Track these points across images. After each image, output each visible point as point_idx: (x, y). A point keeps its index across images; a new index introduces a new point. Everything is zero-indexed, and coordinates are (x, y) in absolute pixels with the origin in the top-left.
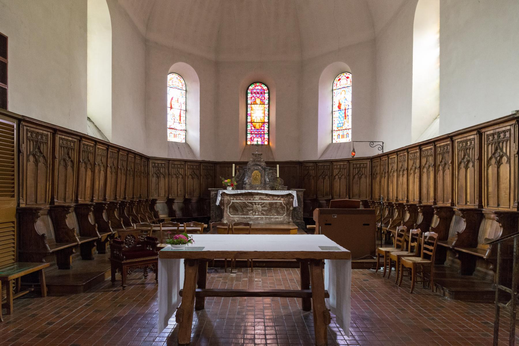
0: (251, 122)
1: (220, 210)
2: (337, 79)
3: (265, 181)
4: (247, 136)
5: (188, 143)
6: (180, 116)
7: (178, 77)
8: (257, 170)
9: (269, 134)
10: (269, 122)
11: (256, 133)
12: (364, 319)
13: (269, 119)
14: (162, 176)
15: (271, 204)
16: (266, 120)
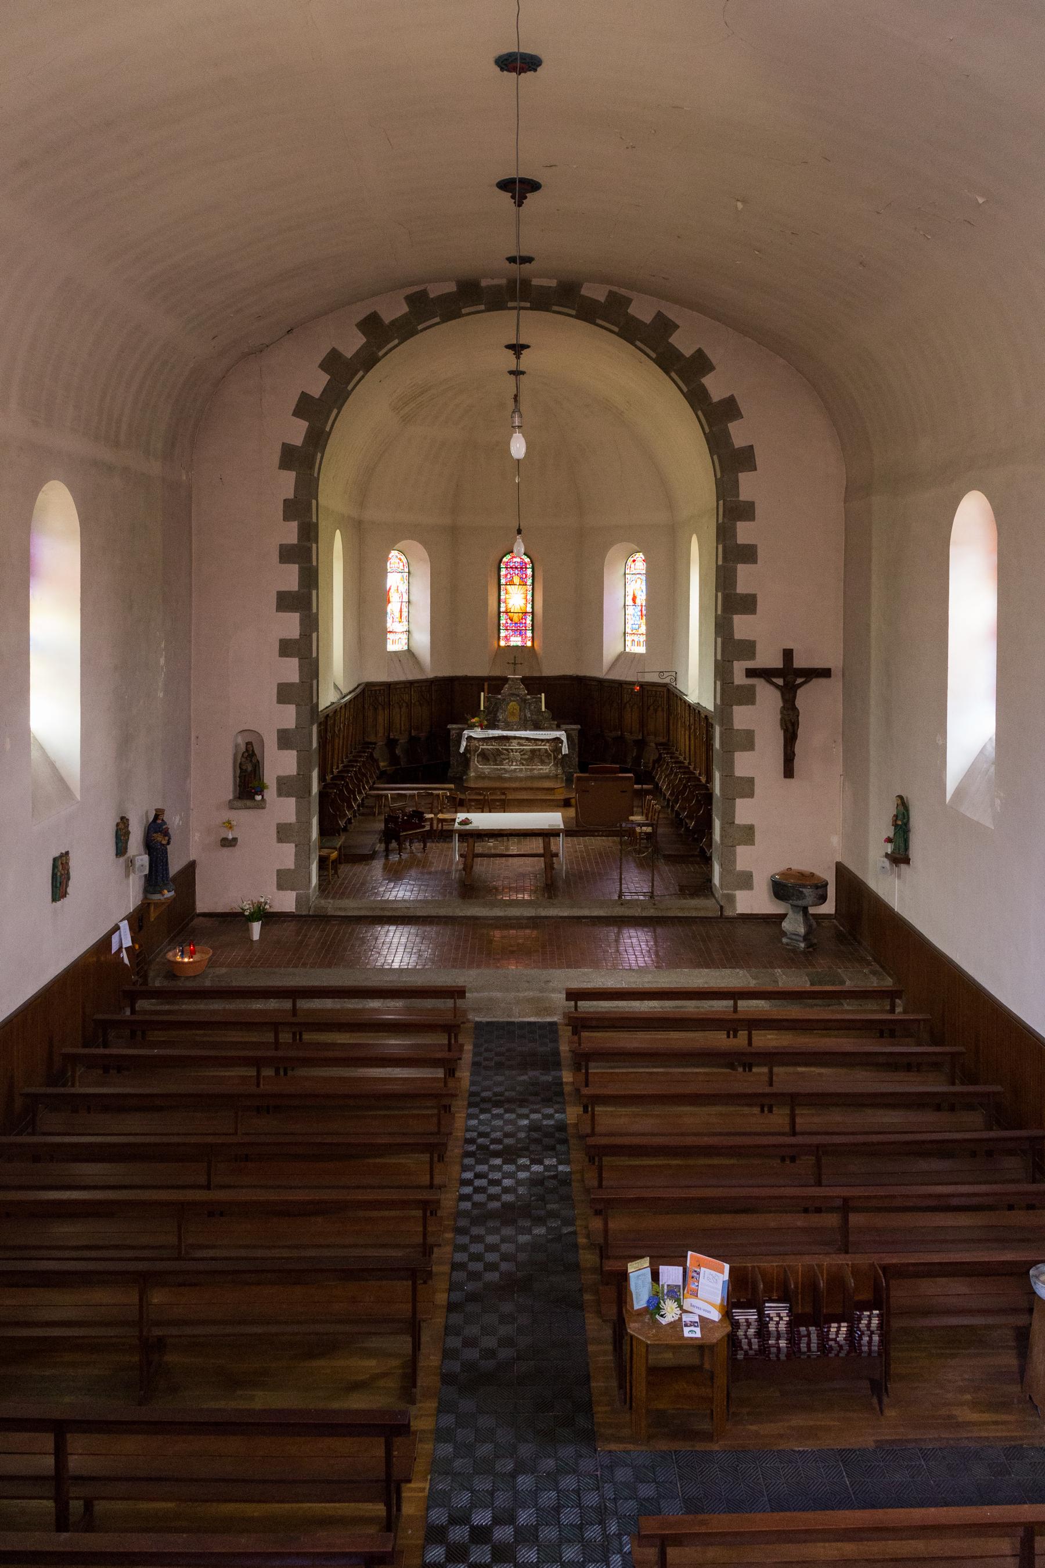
0: (506, 612)
1: (465, 760)
2: (631, 560)
3: (525, 716)
4: (499, 633)
5: (413, 650)
6: (401, 612)
7: (398, 555)
8: (514, 701)
9: (533, 630)
10: (533, 613)
11: (514, 628)
12: (471, 823)
13: (533, 608)
14: (380, 708)
15: (533, 751)
16: (529, 609)
